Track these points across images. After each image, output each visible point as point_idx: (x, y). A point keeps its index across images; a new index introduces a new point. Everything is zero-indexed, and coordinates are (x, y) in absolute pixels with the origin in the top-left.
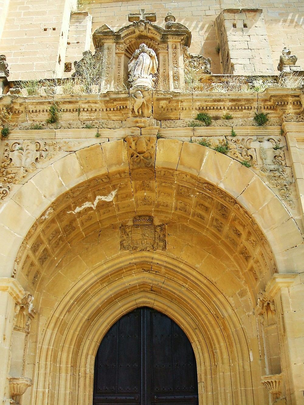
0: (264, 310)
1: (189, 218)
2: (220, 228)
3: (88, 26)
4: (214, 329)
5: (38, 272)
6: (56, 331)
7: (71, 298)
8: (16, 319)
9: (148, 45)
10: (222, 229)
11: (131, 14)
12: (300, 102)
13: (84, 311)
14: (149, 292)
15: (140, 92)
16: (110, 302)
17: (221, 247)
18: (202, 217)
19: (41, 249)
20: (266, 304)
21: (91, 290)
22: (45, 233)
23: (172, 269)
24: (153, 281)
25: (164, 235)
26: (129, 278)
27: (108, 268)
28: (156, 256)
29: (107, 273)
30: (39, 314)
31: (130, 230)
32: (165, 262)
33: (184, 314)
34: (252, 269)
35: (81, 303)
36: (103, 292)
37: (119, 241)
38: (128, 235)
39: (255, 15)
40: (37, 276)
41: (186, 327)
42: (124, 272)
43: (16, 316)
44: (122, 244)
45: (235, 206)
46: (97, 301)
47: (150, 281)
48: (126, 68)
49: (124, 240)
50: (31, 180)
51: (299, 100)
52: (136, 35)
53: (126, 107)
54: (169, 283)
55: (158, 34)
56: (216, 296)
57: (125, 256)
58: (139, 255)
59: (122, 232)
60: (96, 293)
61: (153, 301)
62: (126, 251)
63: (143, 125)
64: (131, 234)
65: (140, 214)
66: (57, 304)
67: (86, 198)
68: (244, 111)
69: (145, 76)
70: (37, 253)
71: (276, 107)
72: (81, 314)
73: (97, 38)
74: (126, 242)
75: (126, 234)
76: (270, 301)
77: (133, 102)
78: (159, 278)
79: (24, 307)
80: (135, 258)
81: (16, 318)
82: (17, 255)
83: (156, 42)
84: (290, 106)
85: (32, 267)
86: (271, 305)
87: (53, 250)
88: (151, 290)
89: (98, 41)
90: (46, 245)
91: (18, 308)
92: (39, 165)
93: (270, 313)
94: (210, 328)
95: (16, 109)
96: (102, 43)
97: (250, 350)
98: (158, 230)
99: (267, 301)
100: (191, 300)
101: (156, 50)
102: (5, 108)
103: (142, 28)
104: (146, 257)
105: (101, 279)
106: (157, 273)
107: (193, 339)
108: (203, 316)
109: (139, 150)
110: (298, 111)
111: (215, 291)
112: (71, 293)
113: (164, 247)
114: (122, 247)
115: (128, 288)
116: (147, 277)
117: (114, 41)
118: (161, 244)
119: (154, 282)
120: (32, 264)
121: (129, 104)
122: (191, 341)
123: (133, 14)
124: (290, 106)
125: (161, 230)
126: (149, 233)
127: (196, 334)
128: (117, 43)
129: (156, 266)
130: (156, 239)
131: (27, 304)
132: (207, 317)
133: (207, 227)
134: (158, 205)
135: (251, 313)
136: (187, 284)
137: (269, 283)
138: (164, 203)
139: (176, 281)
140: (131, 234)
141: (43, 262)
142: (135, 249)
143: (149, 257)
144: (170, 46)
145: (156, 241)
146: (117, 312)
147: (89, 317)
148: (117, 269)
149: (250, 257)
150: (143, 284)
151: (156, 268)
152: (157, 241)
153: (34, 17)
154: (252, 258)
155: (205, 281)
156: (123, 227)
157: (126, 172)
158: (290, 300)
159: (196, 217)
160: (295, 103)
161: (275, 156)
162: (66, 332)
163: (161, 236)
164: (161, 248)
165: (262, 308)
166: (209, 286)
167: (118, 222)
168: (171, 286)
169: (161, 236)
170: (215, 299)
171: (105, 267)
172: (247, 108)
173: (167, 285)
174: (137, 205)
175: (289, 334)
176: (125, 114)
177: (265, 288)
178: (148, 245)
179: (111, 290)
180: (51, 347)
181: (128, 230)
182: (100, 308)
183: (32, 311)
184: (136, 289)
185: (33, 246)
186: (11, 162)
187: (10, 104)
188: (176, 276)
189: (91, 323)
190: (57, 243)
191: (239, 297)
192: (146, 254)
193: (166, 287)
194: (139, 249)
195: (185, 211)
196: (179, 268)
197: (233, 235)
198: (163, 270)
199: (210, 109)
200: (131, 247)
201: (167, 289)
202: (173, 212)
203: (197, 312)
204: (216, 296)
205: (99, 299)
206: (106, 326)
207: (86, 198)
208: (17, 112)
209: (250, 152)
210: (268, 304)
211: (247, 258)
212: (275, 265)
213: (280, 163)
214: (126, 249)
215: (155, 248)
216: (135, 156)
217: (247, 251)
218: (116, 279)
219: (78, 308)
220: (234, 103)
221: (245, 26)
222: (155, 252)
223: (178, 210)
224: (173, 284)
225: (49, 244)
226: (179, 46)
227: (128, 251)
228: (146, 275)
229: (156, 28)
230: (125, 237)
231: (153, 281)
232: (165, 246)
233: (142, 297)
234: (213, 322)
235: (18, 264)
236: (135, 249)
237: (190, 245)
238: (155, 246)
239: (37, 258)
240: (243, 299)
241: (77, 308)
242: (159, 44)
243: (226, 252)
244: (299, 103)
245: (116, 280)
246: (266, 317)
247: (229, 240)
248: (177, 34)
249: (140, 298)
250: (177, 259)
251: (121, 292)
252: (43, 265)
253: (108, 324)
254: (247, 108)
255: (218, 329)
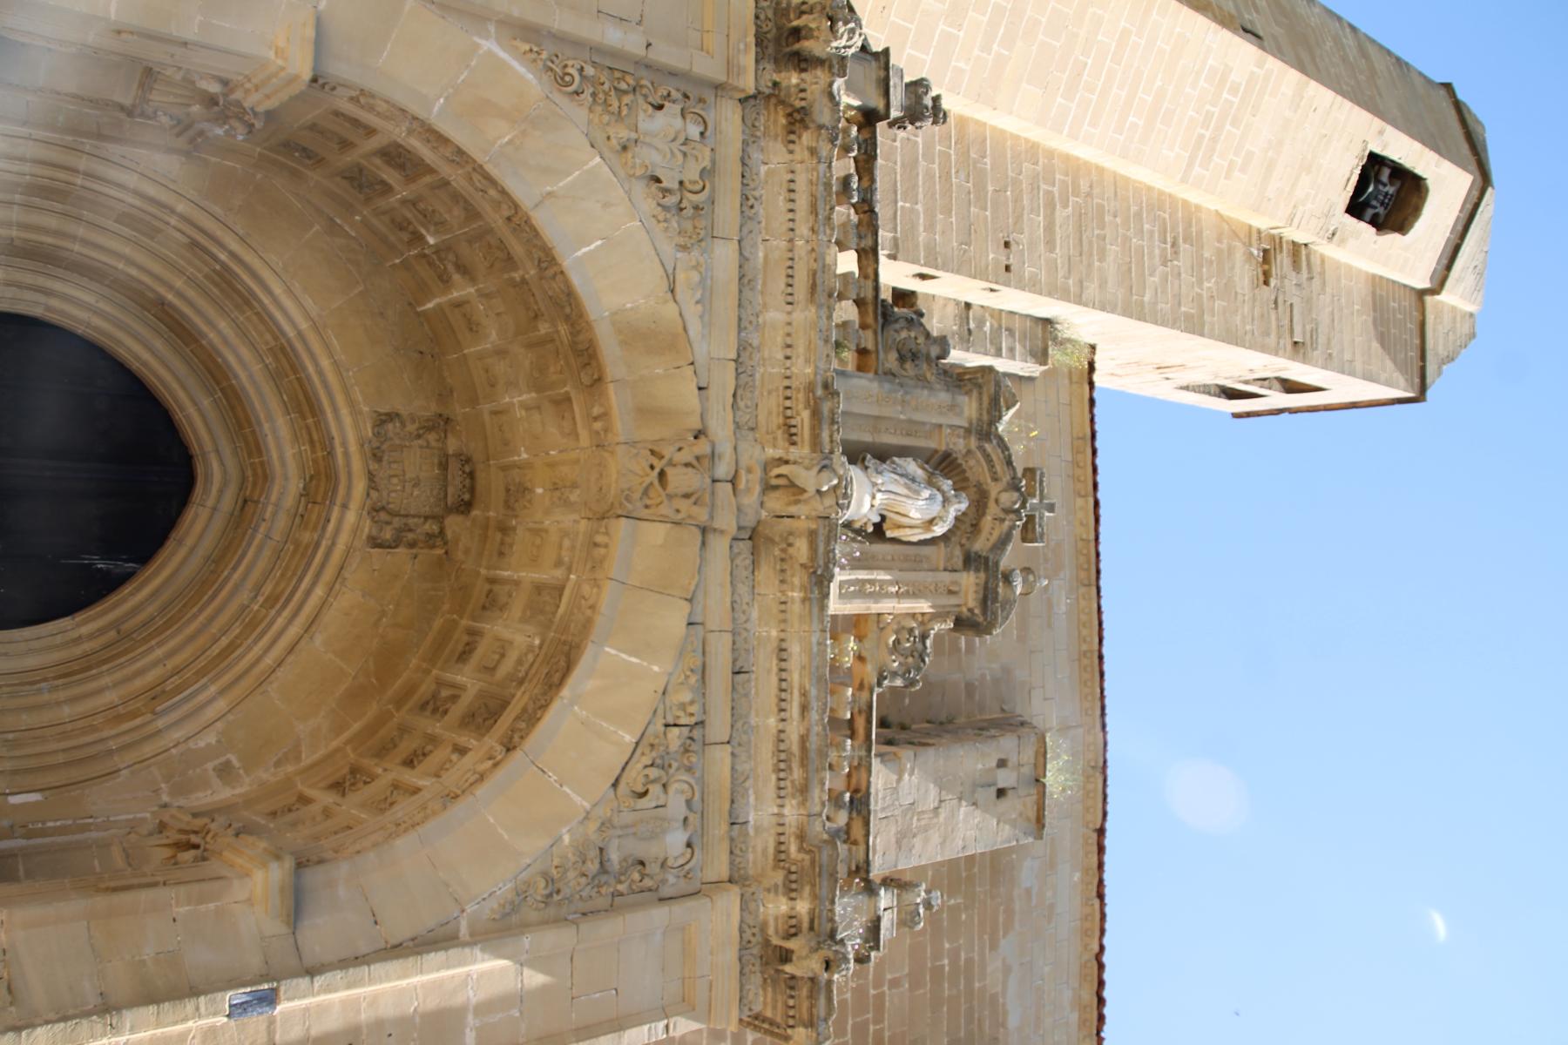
0: (175, 837)
1: (461, 618)
2: (430, 707)
3: (1011, 362)
4: (116, 685)
5: (317, 160)
6: (130, 199)
7: (233, 255)
8: (178, 77)
9: (962, 518)
10: (428, 713)
11: (1042, 475)
12: (795, 935)
13: (191, 293)
14: (239, 495)
15: (835, 482)
16: (214, 373)
17: (372, 710)
18: (464, 656)
19: (391, 176)
20: (194, 839)
21: (255, 318)
22: (437, 191)
23: (309, 564)
24: (276, 505)
25: (412, 545)
26: (284, 431)
27: (320, 373)
28: (351, 517)
29: (304, 369)
30: (187, 154)
31: (433, 444)
32: (334, 544)
33: (166, 596)
34: (304, 800)
35: (216, 285)
36: (246, 353)
37: (404, 412)
38: (419, 436)
39: (1028, 819)
40: (309, 158)
41: (124, 600)
42: (304, 418)
43: (189, 82)
44: (391, 417)
45: (499, 748)
46: (219, 332)
47: (273, 498)
48: (904, 452)
49: (403, 425)
50: (598, 159)
51: (801, 931)
52: (987, 484)
53: (794, 444)
54: (267, 553)
55: (989, 544)
56: (221, 692)
57: (356, 425)
58: (357, 465)
59: (428, 420)
60: (243, 334)
61: (210, 502)
62: (370, 430)
63: (742, 485)
64: (421, 447)
65: (481, 477)
66: (218, 211)
67: (536, 316)
68: (774, 777)
69: (877, 502)
70: (378, 161)
71: (783, 868)
72: (179, 284)
73: (983, 376)
74: (398, 430)
75: (421, 432)
76: (205, 850)
77: (807, 462)
78: (282, 522)
79: (216, 109)
80: (346, 454)
81: (184, 79)
82: (381, 99)
83: (968, 539)
84: (783, 906)
85: (338, 144)
86: (193, 852)
87: (384, 213)
88: (245, 501)
89: (976, 378)
90: (403, 192)
91: (214, 88)
92: (639, 188)
93: (168, 852)
94: (118, 675)
95: (800, 137)
96: (971, 391)
97: (47, 793)
98: (434, 527)
99: (206, 843)
100: (211, 619)
101: (945, 537)
102: (803, 104)
103: (1008, 498)
104: (349, 487)
105: (289, 349)
106: (300, 519)
107: (85, 622)
108: (159, 652)
109: (670, 472)
110: (771, 931)
111: (238, 691)
112: (249, 258)
113: (379, 541)
114: (383, 418)
115: (257, 429)
116: (287, 486)
117: (974, 422)
118: (388, 534)
119: (270, 509)
120: (345, 145)
121: (802, 451)
122: (80, 617)
123: (1041, 482)
124: (783, 906)
125: (430, 536)
126: (419, 499)
127: (102, 631)
128: (968, 431)
129: (319, 516)
130: (404, 520)
131: (223, 118)
132: (155, 664)
133: (435, 672)
134: (504, 529)
135: (165, 798)
136: (261, 606)
137: (263, 844)
138: (511, 546)
139: (272, 574)
140: (421, 447)
141: (350, 179)
142: (377, 456)
143: (348, 495)
144: (956, 576)
145: (397, 519)
146: (181, 395)
147: (171, 305)
148: (318, 400)
149: (344, 795)
150: (265, 477)
151: (314, 517)
152: (397, 522)
153: (1041, 218)
154: (338, 799)
155: (269, 660)
156: (442, 424)
157: (610, 435)
158: (212, 906)
159: (466, 638)
160: (793, 922)
161: (642, 863)
162: (126, 231)
163: (410, 536)
164: (374, 533)
165: (182, 831)
166: (256, 671)
167: (459, 410)
168: (256, 558)
169: (410, 536)
170: (213, 689)
171: (325, 363)
172: (782, 784)
173: (260, 548)
174: (505, 468)
175: (101, 902)
176: (775, 439)
177: (250, 833)
178: (385, 494)
179: (251, 376)
180: (79, 181)
181: (432, 437)
182: (197, 341)
183: (201, 133)
184: (250, 455)
185: (400, 150)
186: (652, 105)
187: (813, 121)
188: (290, 573)
189: (149, 311)
190: (405, 225)
191: (216, 762)
192: (360, 486)
193: (256, 542)
194: (373, 466)
195: (484, 608)
196: (314, 584)
197: (407, 746)
198: (306, 537)
199: (782, 680)
200: (382, 443)
201: (249, 545)
202: (483, 571)
203: (172, 636)
204: (221, 692)
205: (226, 341)
206: (138, 358)
207: (536, 316)
208: (792, 137)
209: (655, 789)
210: (196, 847)
211: (338, 786)
212: (321, 862)
213: (623, 878)
214: (376, 430)
215: (375, 514)
216: (655, 462)
217: (360, 785)
218: (287, 395)
219: (200, 276)
220: (795, 749)
221: (1001, 793)
222: (365, 513)
223: (487, 587)
224: (262, 564)
225: (404, 202)
226: (953, 600)
227: (370, 434)
228: (295, 486)
229: (1004, 541)
230: (411, 428)
231: (276, 505)
232: (380, 546)
233: (225, 472)
234: (138, 683)
235: (352, 99)
236: (374, 455)
237: (380, 619)
238: (383, 516)
239: (363, 162)
240: (211, 773)
241: (200, 271)
242: (962, 546)
243: (356, 726)
244: (793, 931)
245: (282, 397)
246: (156, 840)
247: (395, 733)
248: (988, 597)
249: (222, 464)
250: (339, 580)
251: (244, 410)
252: (338, 179)
253: (145, 364)
254: (782, 784)
255: (116, 699)
